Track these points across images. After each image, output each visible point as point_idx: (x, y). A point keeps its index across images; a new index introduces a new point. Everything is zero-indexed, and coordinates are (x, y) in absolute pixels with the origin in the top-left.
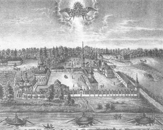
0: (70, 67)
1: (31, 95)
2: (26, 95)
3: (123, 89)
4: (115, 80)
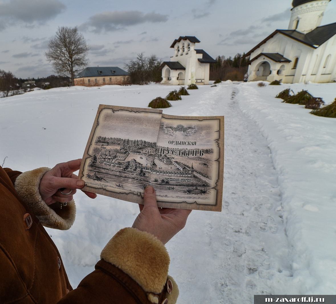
0: (146, 153)
1: (110, 164)
2: (106, 163)
3: (179, 172)
4: (172, 166)
